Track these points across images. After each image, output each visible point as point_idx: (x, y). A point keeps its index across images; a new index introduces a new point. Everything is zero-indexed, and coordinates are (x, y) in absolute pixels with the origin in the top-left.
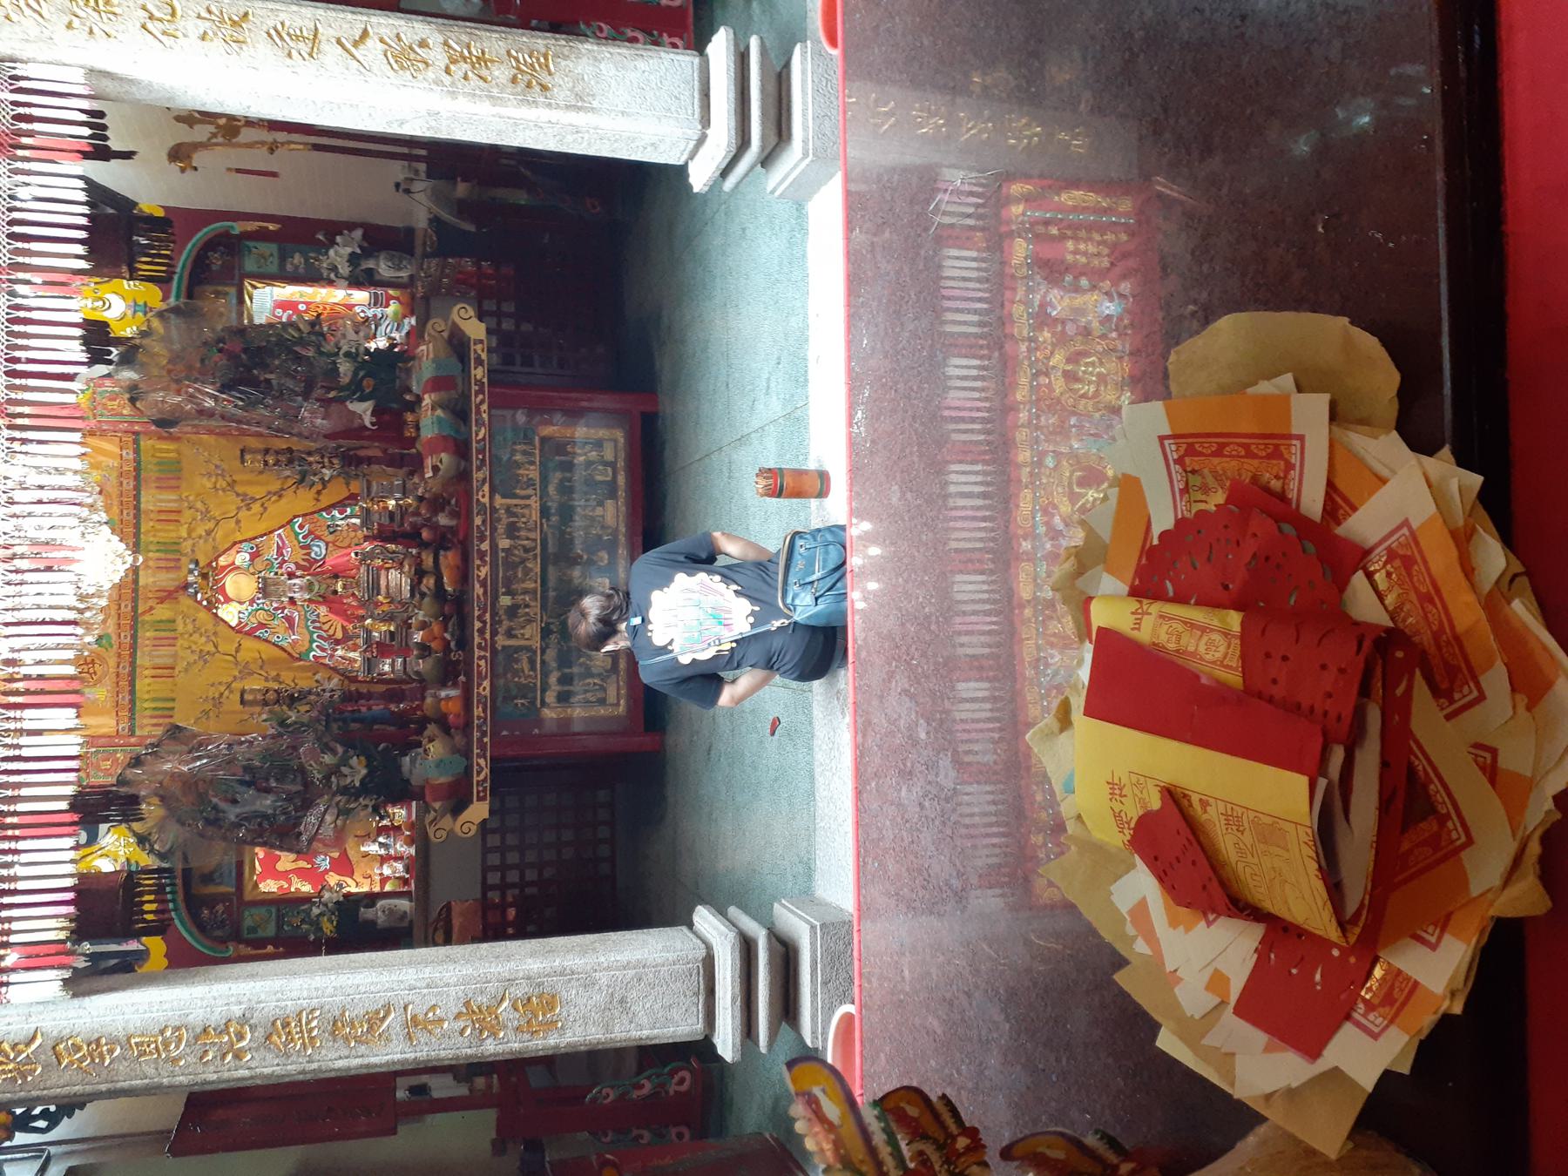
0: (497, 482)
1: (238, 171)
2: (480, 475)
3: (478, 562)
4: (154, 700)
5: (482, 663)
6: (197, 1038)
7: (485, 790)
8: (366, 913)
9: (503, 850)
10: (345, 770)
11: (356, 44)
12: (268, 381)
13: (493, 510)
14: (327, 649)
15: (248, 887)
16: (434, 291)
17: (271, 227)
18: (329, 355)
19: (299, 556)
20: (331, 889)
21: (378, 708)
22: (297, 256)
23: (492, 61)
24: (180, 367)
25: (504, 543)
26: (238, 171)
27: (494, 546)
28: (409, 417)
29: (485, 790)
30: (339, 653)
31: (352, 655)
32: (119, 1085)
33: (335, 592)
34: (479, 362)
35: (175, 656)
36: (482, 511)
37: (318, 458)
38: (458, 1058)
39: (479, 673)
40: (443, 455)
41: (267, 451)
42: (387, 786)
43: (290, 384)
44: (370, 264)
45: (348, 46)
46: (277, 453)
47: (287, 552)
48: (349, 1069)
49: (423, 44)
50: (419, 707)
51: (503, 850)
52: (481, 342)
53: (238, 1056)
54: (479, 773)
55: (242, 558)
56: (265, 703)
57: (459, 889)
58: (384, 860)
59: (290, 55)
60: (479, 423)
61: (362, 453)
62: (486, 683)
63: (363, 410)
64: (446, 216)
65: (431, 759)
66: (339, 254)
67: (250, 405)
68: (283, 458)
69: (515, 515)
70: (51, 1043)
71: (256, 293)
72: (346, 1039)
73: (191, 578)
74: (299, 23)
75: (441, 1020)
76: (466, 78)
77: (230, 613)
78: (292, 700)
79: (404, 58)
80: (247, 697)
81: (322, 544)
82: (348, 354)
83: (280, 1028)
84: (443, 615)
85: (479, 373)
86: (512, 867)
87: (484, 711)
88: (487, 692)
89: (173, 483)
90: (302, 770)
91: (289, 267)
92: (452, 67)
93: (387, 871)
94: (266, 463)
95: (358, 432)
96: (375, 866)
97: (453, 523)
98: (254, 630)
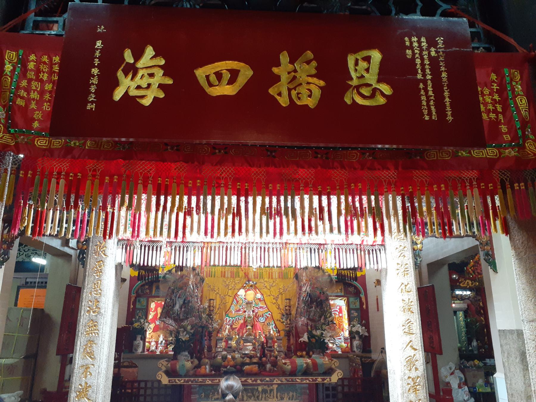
0: (282, 386)
1: (377, 299)
2: (284, 380)
3: (253, 379)
4: (215, 272)
5: (217, 381)
6: (96, 299)
7: (172, 382)
8: (139, 337)
9: (152, 388)
10: (185, 333)
11: (411, 346)
12: (312, 307)
13: (272, 385)
14: (228, 325)
15: (153, 299)
16: (351, 360)
17: (364, 306)
18: (322, 327)
19: (260, 314)
20: (148, 325)
21: (206, 343)
22: (357, 314)
23: (416, 393)
24: (314, 281)
25: (260, 389)
26: (377, 299)
27: (259, 385)
28: (304, 353)
29: (172, 382)
30: (228, 327)
31: (227, 331)
32: (87, 278)
33: (247, 326)
34: (323, 380)
35: (228, 278)
36: (271, 381)
37: (289, 323)
38: (72, 383)
39: (214, 380)
40: (290, 367)
41: (290, 307)
42: (179, 346)
43: (312, 314)
44: (357, 338)
45: (410, 344)
46: (290, 310)
47: (261, 310)
48: (76, 346)
49: (416, 369)
50: (205, 357)
51: (152, 388)
52: (330, 380)
53: (88, 311)
54: (178, 380)
55: (259, 296)
56: (209, 306)
57: (141, 372)
58: (157, 342)
59: (403, 326)
60: (302, 380)
61: (291, 337)
62: (210, 382)
63: (305, 338)
64: (375, 366)
65: (185, 362)
66: (359, 328)
67: (305, 302)
68: (288, 312)
69: (270, 392)
70: (103, 260)
71: (343, 301)
72: (87, 345)
73: (251, 282)
74: (414, 328)
75: (86, 377)
76: (408, 384)
77: (242, 292)
78: (209, 315)
79: (410, 362)
80: (212, 301)
81: (264, 321)
82: (322, 334)
83: (94, 324)
84: (236, 366)
85: (319, 380)
86: (145, 392)
87: (200, 382)
88: (207, 383)
89: (281, 276)
90: (187, 318)
91: (352, 311)
92: (411, 379)
93: (153, 343)
94: (286, 306)
95: (298, 336)
96: (155, 340)
97: (268, 369)
98: (236, 300)
